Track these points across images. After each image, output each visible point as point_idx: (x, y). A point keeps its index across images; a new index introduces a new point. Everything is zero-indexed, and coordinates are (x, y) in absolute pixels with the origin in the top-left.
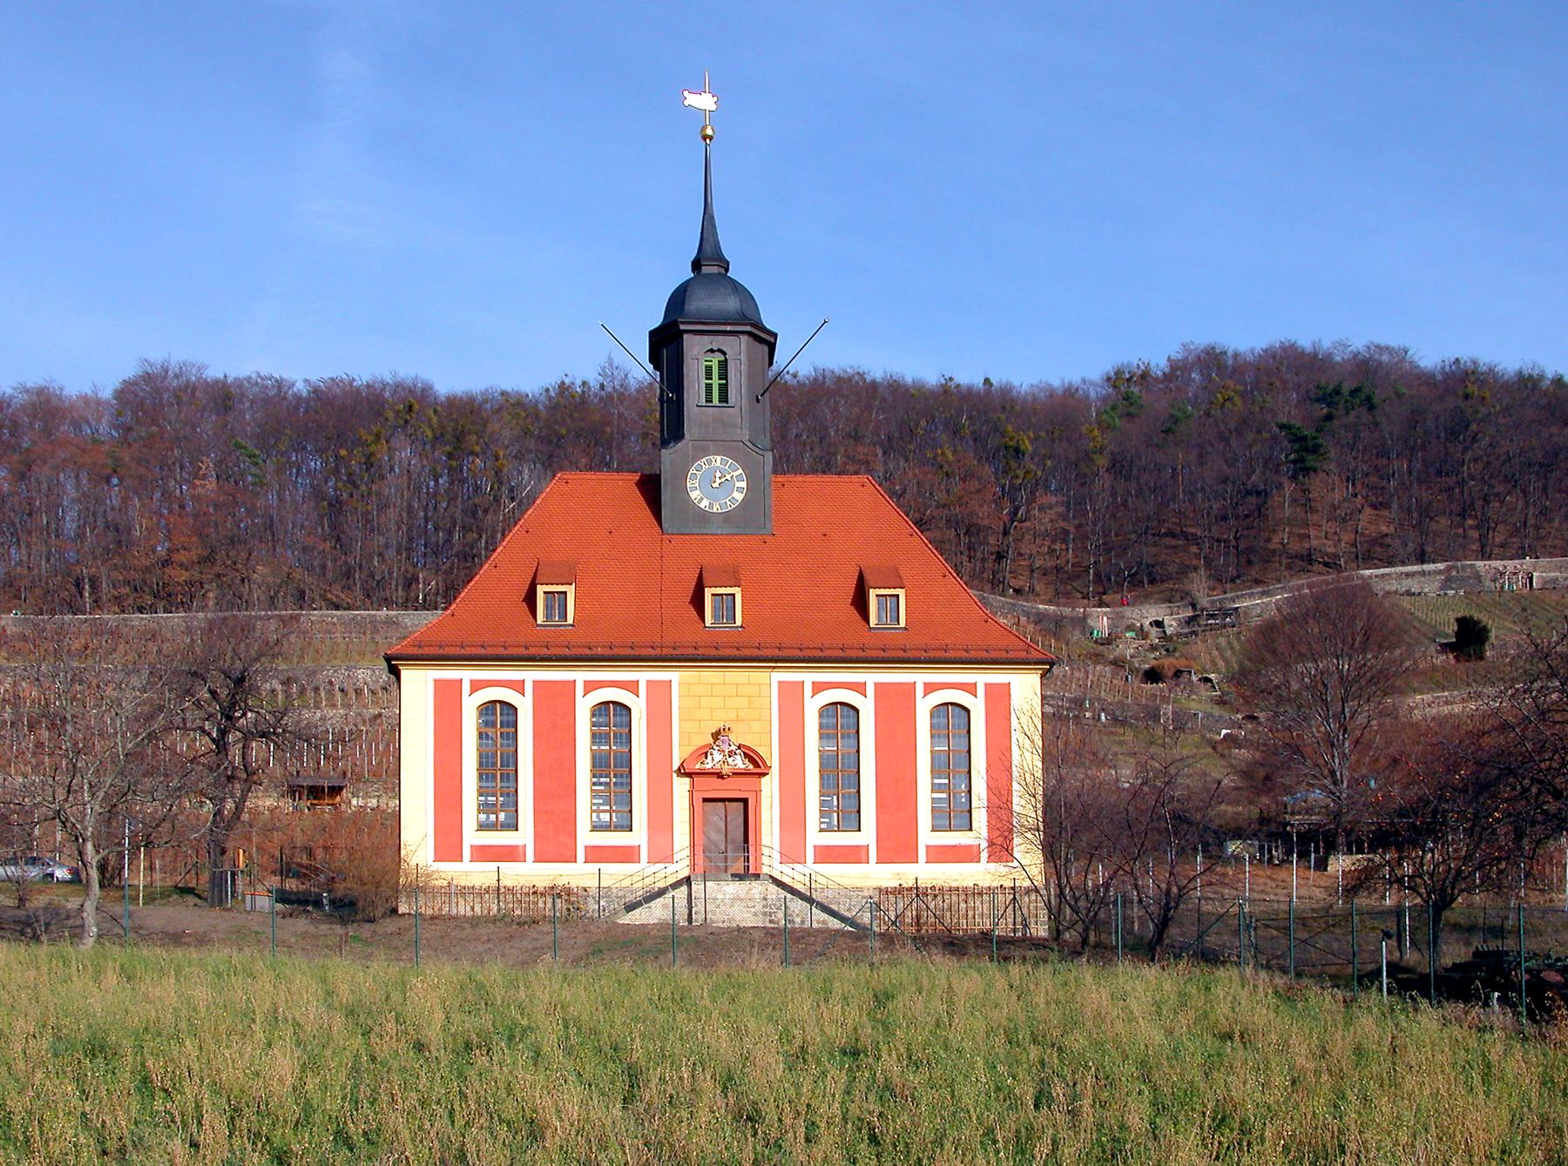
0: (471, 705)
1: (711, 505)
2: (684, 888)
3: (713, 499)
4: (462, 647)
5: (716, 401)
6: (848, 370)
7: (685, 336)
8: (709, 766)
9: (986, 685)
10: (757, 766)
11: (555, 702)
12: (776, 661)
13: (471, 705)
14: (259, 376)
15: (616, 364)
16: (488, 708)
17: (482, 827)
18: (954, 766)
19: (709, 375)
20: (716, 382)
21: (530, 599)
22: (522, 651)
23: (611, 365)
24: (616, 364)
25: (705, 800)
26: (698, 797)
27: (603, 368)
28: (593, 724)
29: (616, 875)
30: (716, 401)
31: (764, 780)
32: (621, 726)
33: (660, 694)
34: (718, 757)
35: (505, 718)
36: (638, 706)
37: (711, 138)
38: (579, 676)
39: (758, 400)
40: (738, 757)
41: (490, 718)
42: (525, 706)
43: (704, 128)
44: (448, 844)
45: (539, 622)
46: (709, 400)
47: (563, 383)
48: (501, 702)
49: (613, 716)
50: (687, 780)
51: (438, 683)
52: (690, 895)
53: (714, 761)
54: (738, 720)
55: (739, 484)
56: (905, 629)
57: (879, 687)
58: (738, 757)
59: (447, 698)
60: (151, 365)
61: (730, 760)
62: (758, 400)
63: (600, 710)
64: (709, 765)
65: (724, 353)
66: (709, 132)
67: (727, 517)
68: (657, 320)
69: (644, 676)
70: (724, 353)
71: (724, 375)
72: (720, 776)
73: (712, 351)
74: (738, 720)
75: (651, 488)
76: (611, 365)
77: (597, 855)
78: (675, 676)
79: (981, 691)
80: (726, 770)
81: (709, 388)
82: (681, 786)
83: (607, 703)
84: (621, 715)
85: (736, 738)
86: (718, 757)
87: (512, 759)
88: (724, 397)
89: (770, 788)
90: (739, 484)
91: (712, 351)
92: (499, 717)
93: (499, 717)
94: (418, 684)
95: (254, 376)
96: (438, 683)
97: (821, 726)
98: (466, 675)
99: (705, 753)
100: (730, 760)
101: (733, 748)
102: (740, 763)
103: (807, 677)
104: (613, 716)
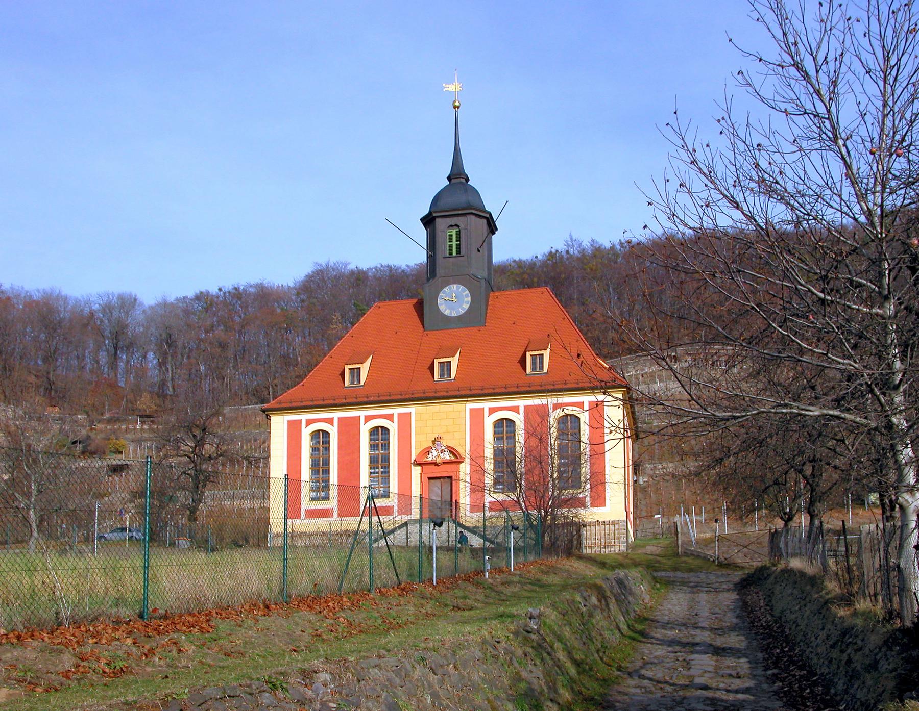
0: (306, 433)
1: (451, 313)
2: (405, 528)
3: (452, 309)
4: (302, 402)
5: (454, 254)
6: (729, 230)
7: (437, 220)
8: (430, 459)
9: (525, 407)
10: (457, 459)
11: (349, 429)
12: (467, 397)
13: (306, 433)
14: (382, 266)
15: (574, 239)
16: (316, 434)
17: (313, 499)
18: (320, 467)
19: (451, 241)
20: (454, 243)
21: (431, 368)
22: (332, 402)
23: (571, 239)
24: (574, 239)
25: (429, 478)
26: (425, 477)
27: (567, 242)
28: (371, 440)
29: (322, 524)
30: (454, 254)
31: (462, 465)
32: (510, 433)
33: (405, 419)
34: (435, 453)
35: (325, 439)
36: (393, 428)
37: (458, 107)
38: (362, 413)
39: (479, 251)
40: (446, 453)
41: (500, 429)
42: (333, 431)
43: (455, 102)
44: (292, 509)
45: (346, 385)
46: (451, 254)
47: (551, 252)
48: (506, 419)
49: (380, 435)
50: (419, 468)
51: (290, 422)
52: (407, 532)
53: (433, 456)
54: (447, 432)
55: (466, 299)
56: (547, 373)
57: (340, 419)
58: (446, 453)
59: (294, 429)
60: (321, 265)
61: (441, 455)
62: (479, 251)
63: (563, 420)
64: (430, 458)
65: (458, 226)
66: (457, 104)
67: (460, 318)
68: (426, 211)
69: (396, 411)
70: (458, 226)
71: (458, 239)
72: (436, 464)
73: (451, 226)
74: (447, 432)
75: (419, 307)
76: (571, 239)
77: (312, 514)
78: (412, 409)
79: (396, 419)
80: (439, 461)
81: (451, 246)
82: (416, 471)
83: (502, 420)
84: (510, 426)
85: (445, 443)
86: (435, 453)
87: (327, 462)
88: (458, 252)
89: (465, 469)
90: (466, 299)
91: (451, 226)
92: (321, 437)
93: (321, 437)
94: (279, 424)
95: (379, 266)
96: (290, 422)
97: (495, 433)
98: (303, 417)
99: (427, 451)
100: (441, 455)
101: (443, 448)
102: (447, 456)
103: (485, 405)
104: (380, 435)
